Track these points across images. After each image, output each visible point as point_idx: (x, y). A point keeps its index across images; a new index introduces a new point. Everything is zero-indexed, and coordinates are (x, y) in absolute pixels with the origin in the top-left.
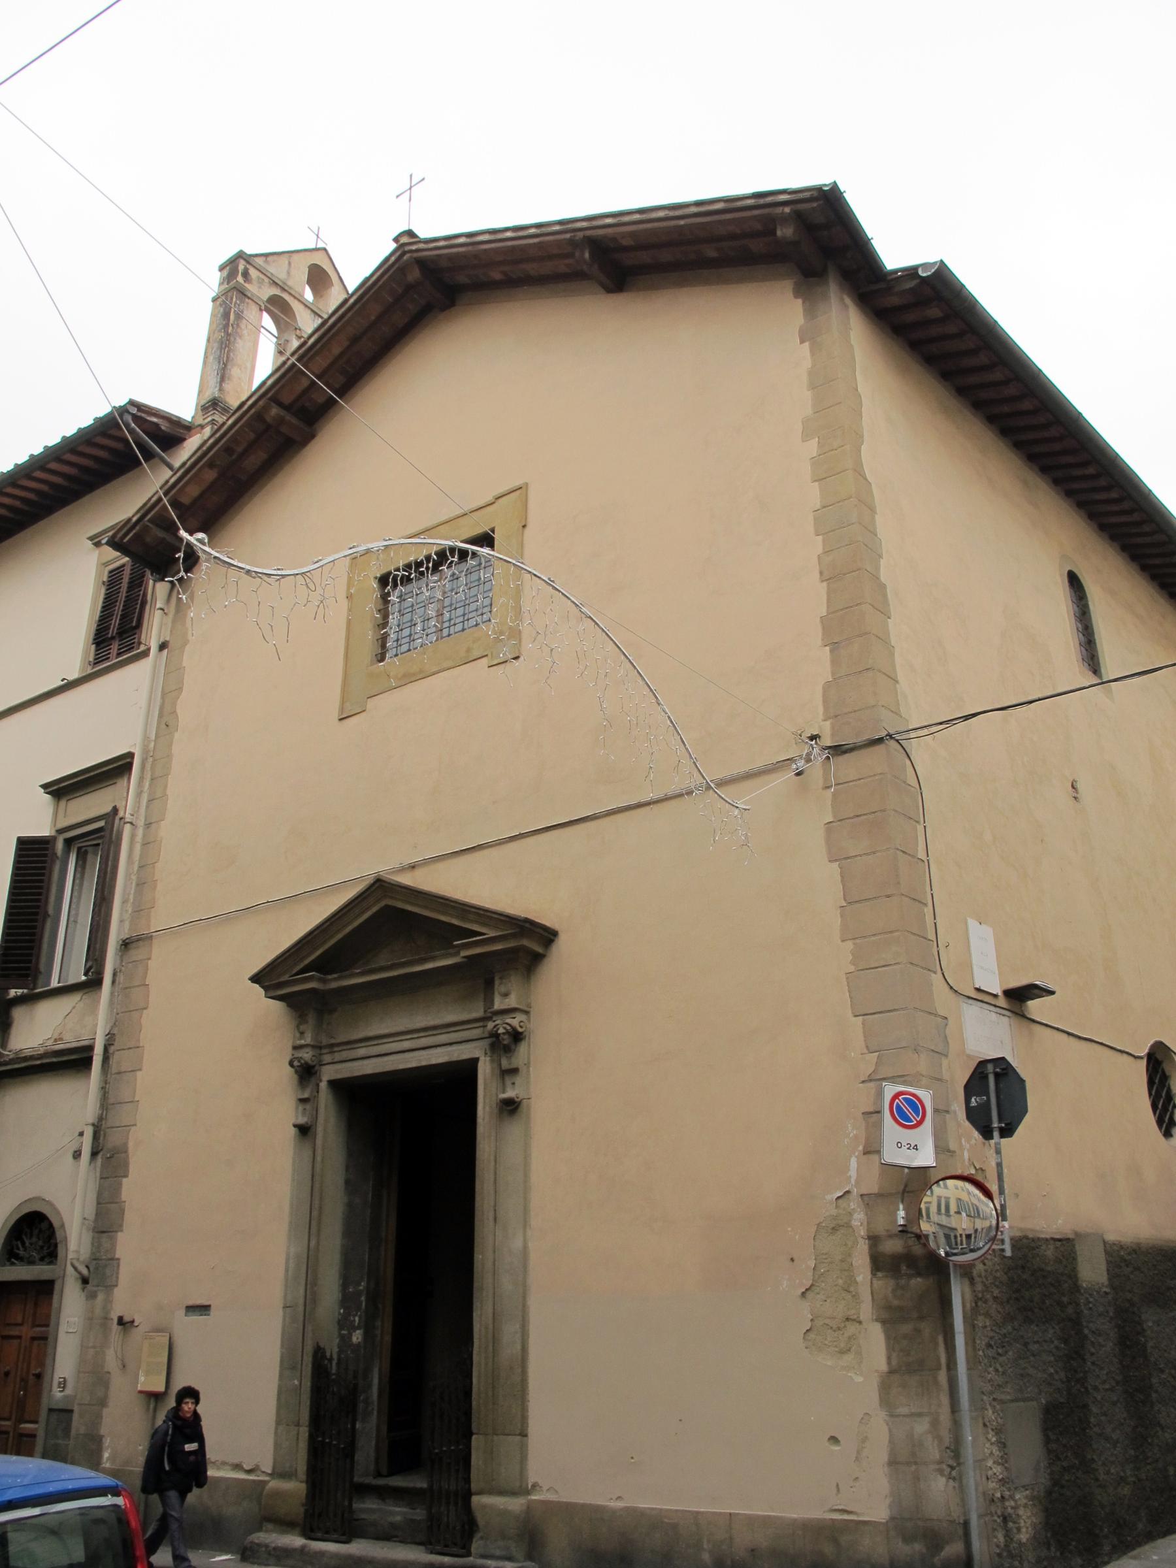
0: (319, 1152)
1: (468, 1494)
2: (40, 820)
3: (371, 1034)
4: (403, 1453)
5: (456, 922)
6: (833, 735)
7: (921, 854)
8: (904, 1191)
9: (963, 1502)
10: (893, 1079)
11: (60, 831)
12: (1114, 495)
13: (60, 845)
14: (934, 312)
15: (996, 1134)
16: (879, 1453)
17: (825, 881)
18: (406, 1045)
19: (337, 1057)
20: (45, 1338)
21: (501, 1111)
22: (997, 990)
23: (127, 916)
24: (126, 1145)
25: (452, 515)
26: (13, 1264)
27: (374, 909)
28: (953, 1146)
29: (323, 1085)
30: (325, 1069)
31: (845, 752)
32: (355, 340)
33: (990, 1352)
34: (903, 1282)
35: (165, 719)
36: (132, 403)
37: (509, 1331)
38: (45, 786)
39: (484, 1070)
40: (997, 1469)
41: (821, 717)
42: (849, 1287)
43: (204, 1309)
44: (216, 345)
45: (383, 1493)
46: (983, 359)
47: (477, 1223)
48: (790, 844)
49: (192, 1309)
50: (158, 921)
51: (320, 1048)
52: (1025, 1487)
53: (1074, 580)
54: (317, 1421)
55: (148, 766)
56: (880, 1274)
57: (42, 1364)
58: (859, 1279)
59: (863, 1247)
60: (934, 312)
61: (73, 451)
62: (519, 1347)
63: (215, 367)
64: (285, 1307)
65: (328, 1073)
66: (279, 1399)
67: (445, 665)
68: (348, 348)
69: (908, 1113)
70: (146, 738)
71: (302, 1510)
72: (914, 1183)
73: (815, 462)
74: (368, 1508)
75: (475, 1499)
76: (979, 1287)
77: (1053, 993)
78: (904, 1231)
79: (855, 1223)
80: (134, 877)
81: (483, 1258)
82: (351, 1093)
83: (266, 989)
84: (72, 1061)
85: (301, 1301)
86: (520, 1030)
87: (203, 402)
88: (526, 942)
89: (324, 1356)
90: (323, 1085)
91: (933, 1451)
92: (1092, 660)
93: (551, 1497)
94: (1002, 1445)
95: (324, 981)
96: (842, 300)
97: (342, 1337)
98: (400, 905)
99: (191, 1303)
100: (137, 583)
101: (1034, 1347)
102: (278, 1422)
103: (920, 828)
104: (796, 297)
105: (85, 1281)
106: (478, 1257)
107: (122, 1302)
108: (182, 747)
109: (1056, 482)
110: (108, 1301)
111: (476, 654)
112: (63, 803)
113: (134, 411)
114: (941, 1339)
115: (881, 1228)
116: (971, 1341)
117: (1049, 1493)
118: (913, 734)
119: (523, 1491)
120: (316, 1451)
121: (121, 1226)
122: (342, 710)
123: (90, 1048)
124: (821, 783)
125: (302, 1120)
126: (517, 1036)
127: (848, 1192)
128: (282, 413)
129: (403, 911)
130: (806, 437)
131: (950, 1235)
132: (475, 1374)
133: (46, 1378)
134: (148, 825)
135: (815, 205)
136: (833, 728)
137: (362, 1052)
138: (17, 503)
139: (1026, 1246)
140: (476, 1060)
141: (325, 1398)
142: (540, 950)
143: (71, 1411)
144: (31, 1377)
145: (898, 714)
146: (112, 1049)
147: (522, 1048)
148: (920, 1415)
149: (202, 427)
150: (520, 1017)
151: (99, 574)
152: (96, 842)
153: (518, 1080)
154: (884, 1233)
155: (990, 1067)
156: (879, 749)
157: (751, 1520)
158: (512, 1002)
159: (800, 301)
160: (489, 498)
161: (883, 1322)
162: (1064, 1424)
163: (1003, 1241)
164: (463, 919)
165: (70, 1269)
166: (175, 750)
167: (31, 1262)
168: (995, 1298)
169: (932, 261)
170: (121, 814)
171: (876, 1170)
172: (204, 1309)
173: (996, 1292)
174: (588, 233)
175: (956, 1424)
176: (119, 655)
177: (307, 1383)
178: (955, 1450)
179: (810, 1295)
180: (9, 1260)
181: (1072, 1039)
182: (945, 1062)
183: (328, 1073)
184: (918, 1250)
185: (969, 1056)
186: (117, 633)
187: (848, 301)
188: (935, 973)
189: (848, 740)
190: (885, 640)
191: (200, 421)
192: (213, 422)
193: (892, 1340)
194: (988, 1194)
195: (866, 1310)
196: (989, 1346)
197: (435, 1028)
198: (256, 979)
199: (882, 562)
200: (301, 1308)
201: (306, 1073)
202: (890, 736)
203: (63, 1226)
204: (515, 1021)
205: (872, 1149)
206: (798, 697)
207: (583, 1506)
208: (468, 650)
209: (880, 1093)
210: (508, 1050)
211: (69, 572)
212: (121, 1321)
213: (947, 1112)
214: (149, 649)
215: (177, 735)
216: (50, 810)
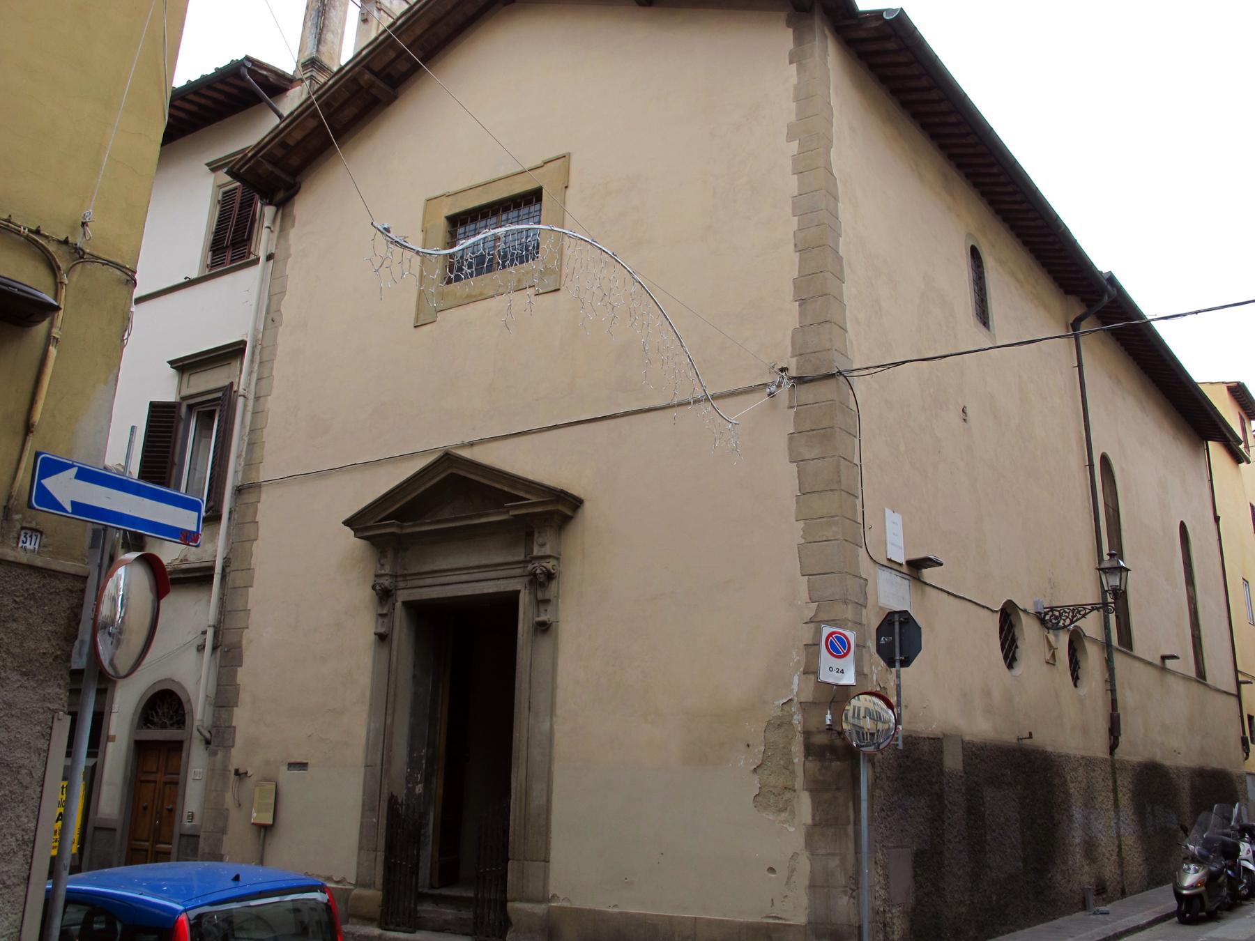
0: (394, 653)
2: (167, 390)
4: (449, 873)
5: (506, 489)
7: (857, 461)
8: (832, 701)
9: (859, 913)
10: (828, 622)
11: (184, 399)
12: (1010, 189)
13: (184, 409)
14: (891, 45)
15: (897, 664)
16: (802, 879)
17: (786, 476)
18: (464, 578)
19: (409, 584)
20: (177, 783)
21: (536, 630)
22: (902, 560)
23: (240, 468)
24: (240, 642)
25: (509, 173)
27: (443, 476)
28: (866, 670)
29: (399, 605)
30: (399, 592)
32: (434, 24)
33: (883, 814)
34: (827, 764)
35: (270, 315)
36: (247, 58)
37: (538, 789)
38: (171, 363)
39: (524, 600)
40: (882, 892)
42: (788, 766)
43: (303, 766)
44: (314, 13)
45: (438, 900)
46: (924, 82)
47: (516, 710)
48: (759, 441)
49: (293, 765)
50: (265, 474)
52: (899, 905)
53: (975, 253)
54: (390, 848)
55: (257, 351)
57: (174, 803)
58: (796, 761)
59: (799, 738)
60: (891, 45)
61: (196, 93)
62: (545, 799)
63: (314, 31)
64: (366, 766)
65: (402, 596)
66: (361, 833)
68: (427, 30)
69: (838, 647)
70: (256, 330)
71: (379, 910)
72: (840, 696)
73: (795, 159)
74: (426, 909)
75: (509, 905)
76: (878, 769)
77: (941, 564)
78: (830, 728)
79: (795, 722)
80: (246, 438)
81: (519, 735)
82: (421, 612)
83: (356, 531)
85: (379, 762)
87: (303, 60)
88: (560, 508)
89: (396, 801)
90: (399, 605)
91: (841, 879)
92: (983, 315)
93: (565, 904)
94: (886, 877)
95: (402, 528)
96: (823, 32)
97: (408, 788)
98: (463, 473)
99: (292, 761)
100: (247, 204)
101: (911, 812)
102: (360, 848)
103: (857, 441)
104: (788, 26)
105: (208, 742)
106: (516, 735)
107: (237, 758)
108: (285, 340)
109: (968, 176)
110: (227, 757)
112: (186, 377)
113: (250, 65)
114: (851, 804)
115: (813, 724)
116: (871, 807)
117: (914, 910)
118: (855, 373)
119: (546, 899)
120: (389, 868)
122: (417, 319)
123: (212, 568)
124: (787, 404)
125: (381, 630)
126: (550, 576)
127: (791, 700)
128: (373, 78)
129: (465, 478)
130: (790, 138)
131: (859, 731)
132: (511, 818)
133: (178, 813)
134: (257, 398)
136: (798, 363)
137: (429, 581)
139: (912, 741)
140: (519, 592)
141: (396, 831)
142: (569, 513)
143: (199, 836)
144: (165, 812)
145: (845, 355)
146: (228, 570)
147: (554, 584)
148: (833, 854)
149: (302, 80)
150: (553, 562)
151: (214, 194)
152: (214, 411)
153: (550, 608)
154: (814, 730)
155: (896, 617)
156: (832, 382)
157: (710, 922)
158: (547, 550)
159: (791, 30)
160: (539, 162)
161: (811, 791)
162: (927, 864)
163: (897, 739)
164: (513, 487)
165: (195, 733)
166: (279, 340)
167: (164, 726)
168: (888, 778)
169: (894, 7)
170: (235, 388)
171: (811, 685)
172: (303, 766)
173: (889, 773)
175: (858, 862)
176: (232, 261)
177: (383, 821)
178: (856, 878)
179: (759, 771)
181: (951, 598)
182: (864, 611)
183: (402, 596)
184: (838, 742)
185: (881, 608)
187: (827, 32)
189: (809, 372)
190: (838, 299)
191: (299, 76)
192: (311, 78)
193: (816, 803)
194: (890, 706)
195: (799, 782)
196: (882, 810)
197: (487, 566)
198: (347, 523)
199: (841, 240)
200: (379, 768)
201: (384, 595)
202: (840, 373)
203: (189, 701)
204: (549, 565)
205: (811, 670)
206: (774, 340)
207: (589, 911)
209: (818, 632)
210: (543, 586)
212: (237, 772)
214: (258, 259)
215: (281, 329)
216: (175, 381)
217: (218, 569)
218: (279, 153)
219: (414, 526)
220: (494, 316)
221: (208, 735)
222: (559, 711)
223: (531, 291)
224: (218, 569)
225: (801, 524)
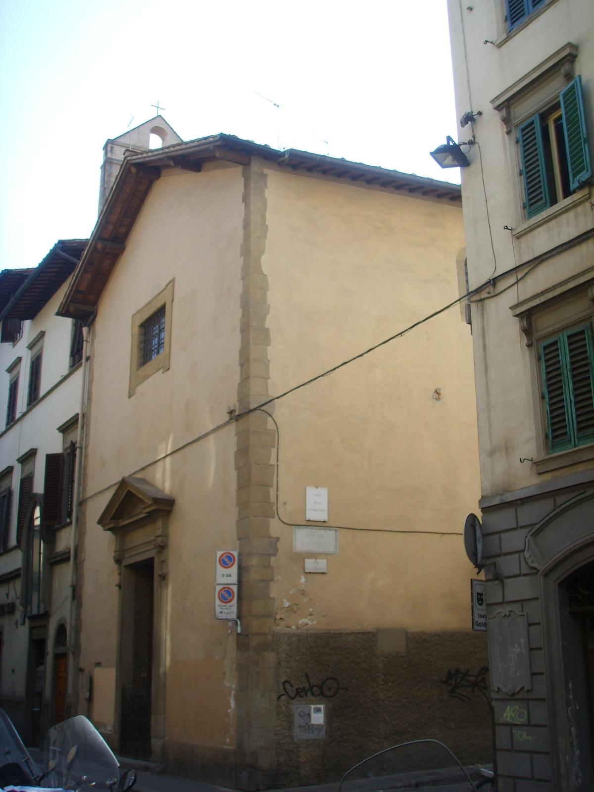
50: (89, 493)
123: (69, 552)
137: (133, 553)
142: (168, 508)
183: (125, 562)
201: (118, 561)
223: (161, 371)
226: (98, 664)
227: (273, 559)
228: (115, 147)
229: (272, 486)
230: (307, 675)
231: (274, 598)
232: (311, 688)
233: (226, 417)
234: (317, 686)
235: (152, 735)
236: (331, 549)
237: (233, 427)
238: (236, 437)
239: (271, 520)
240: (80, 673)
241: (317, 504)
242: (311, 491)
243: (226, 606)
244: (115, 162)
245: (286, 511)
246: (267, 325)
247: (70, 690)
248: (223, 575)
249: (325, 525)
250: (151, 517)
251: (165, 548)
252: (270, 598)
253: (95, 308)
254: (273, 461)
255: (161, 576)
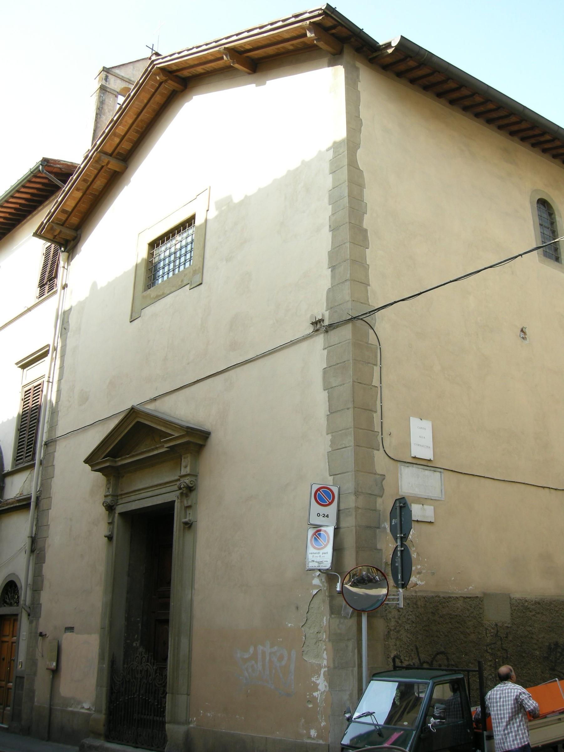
1: (163, 723)
3: (136, 488)
6: (329, 319)
24: (44, 547)
26: (5, 606)
29: (117, 515)
31: (337, 327)
39: (177, 505)
41: (325, 309)
50: (60, 432)
51: (117, 496)
56: (333, 616)
65: (120, 509)
67: (173, 290)
75: (167, 726)
82: (130, 518)
84: (22, 505)
86: (191, 485)
100: (55, 254)
105: (29, 615)
110: (37, 624)
111: (185, 283)
121: (42, 588)
122: (131, 318)
123: (30, 498)
135: (321, 18)
137: (133, 498)
138: (7, 215)
142: (200, 442)
147: (193, 494)
174: (227, 46)
176: (48, 292)
180: (3, 604)
183: (120, 509)
186: (48, 280)
188: (378, 450)
197: (160, 485)
201: (110, 508)
208: (182, 281)
211: (29, 248)
213: (378, 528)
215: (69, 334)
217: (33, 499)
218: (63, 217)
219: (122, 460)
220: (172, 308)
221: (28, 610)
222: (196, 586)
223: (188, 287)
224: (33, 499)
225: (330, 437)
226: (70, 629)
227: (379, 500)
228: (110, 76)
229: (376, 412)
230: (417, 648)
231: (381, 550)
232: (422, 664)
233: (311, 329)
234: (427, 663)
235: (167, 718)
236: (435, 493)
237: (320, 340)
238: (325, 352)
239: (375, 452)
240: (40, 638)
241: (421, 439)
242: (414, 422)
243: (319, 553)
244: (108, 90)
245: (391, 444)
246: (365, 226)
247: (22, 657)
248: (318, 515)
249: (430, 464)
250: (175, 454)
251: (193, 490)
252: (378, 550)
253: (79, 232)
254: (376, 382)
255: (186, 523)
